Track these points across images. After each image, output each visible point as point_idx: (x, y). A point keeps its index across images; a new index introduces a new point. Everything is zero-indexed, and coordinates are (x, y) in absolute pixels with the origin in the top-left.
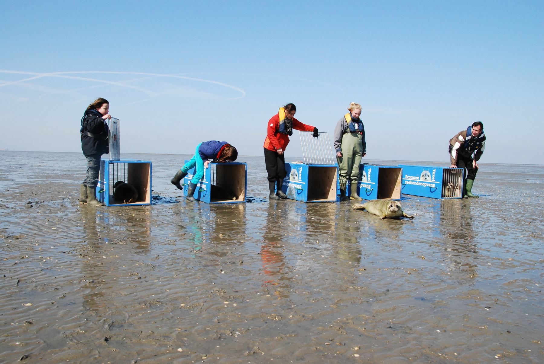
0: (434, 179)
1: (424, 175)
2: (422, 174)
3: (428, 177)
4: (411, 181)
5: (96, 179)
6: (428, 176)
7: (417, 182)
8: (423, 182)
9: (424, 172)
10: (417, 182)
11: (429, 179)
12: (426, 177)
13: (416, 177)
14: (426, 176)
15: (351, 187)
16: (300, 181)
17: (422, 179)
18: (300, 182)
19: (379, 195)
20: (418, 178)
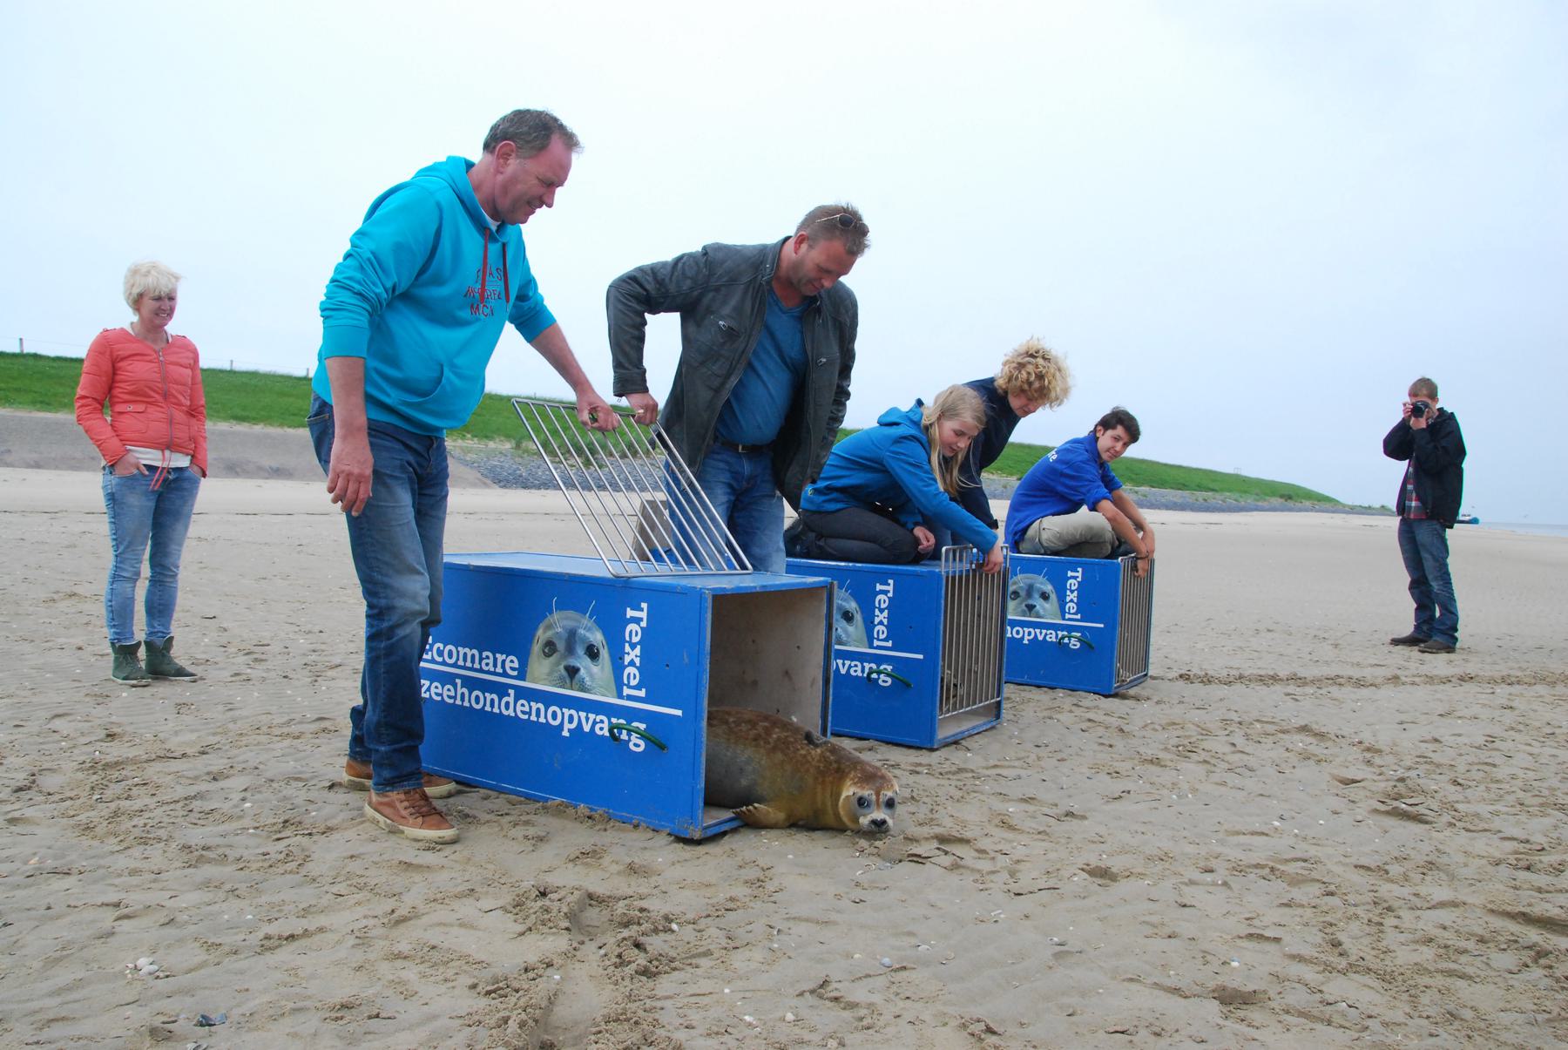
0: (634, 683)
1: (561, 646)
2: (541, 635)
3: (588, 660)
4: (458, 681)
5: (714, 709)
6: (1045, 596)
7: (501, 690)
8: (548, 699)
9: (558, 622)
10: (501, 690)
11: (596, 674)
12: (1030, 602)
13: (500, 657)
14: (570, 650)
15: (181, 455)
16: (1067, 616)
17: (542, 674)
18: (630, 698)
19: (208, 373)
20: (512, 662)
